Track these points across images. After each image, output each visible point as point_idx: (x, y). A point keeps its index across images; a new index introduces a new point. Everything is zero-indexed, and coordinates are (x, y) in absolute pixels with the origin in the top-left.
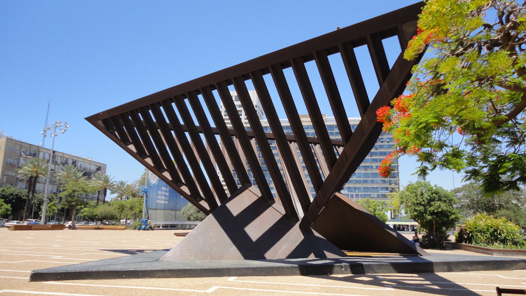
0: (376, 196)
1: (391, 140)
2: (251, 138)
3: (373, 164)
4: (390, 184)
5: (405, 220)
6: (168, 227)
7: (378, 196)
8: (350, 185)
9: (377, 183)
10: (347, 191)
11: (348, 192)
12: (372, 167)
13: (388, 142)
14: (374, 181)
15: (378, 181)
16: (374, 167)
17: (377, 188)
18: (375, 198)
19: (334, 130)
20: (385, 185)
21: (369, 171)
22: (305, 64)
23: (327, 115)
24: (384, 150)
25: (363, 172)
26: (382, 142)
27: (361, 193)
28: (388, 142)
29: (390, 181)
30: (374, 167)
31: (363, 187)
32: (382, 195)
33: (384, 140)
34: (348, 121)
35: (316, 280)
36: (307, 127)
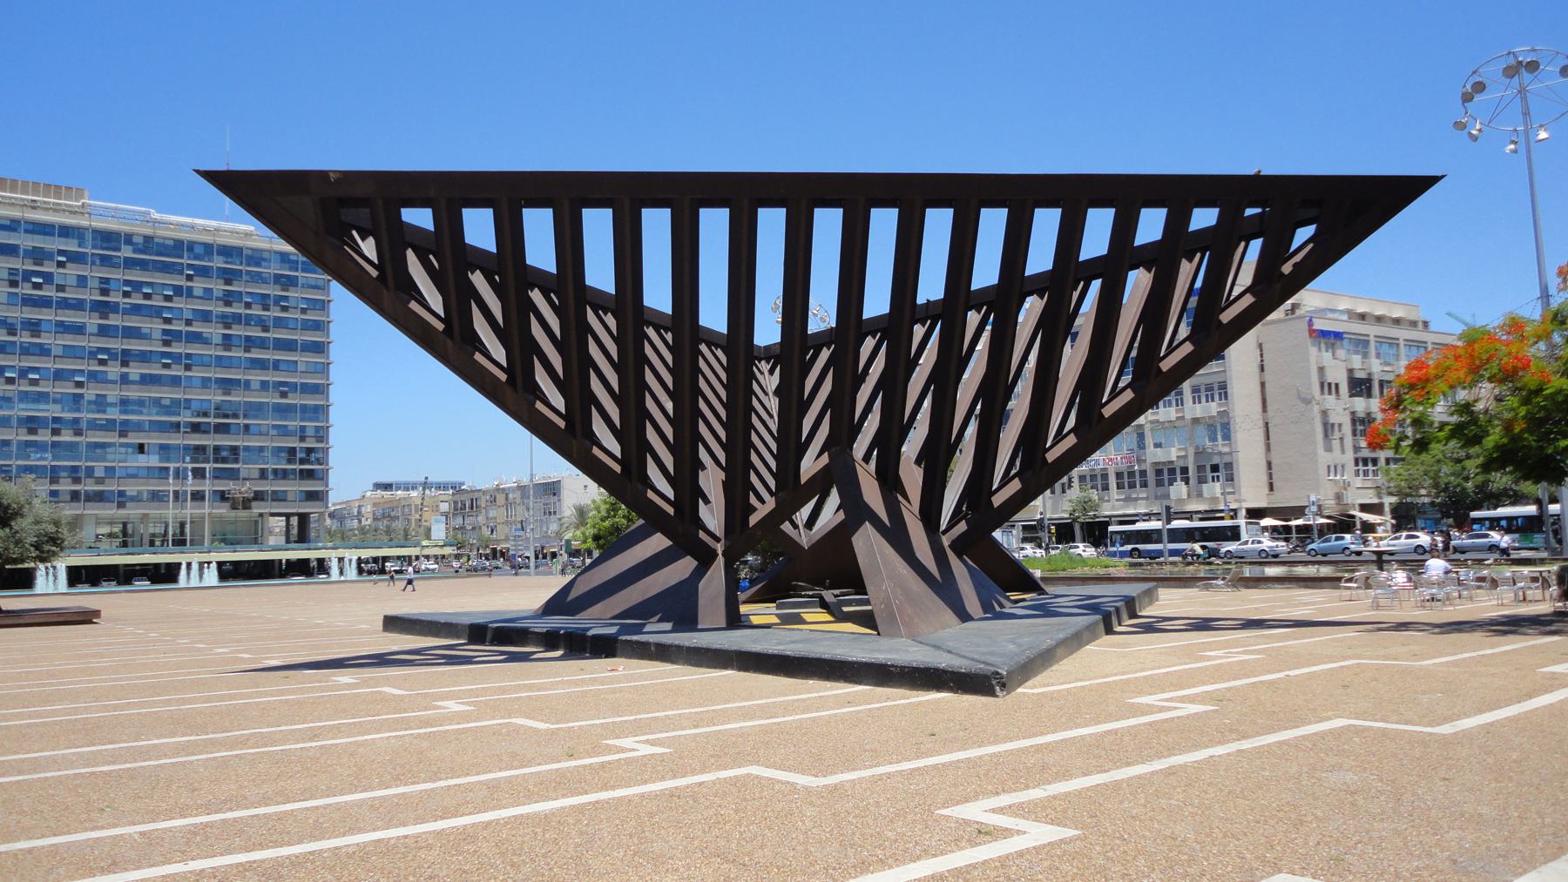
0: (256, 474)
1: (311, 307)
2: (768, 353)
3: (251, 375)
4: (302, 439)
5: (377, 544)
6: (1271, 473)
7: (263, 474)
8: (170, 439)
9: (260, 434)
10: (157, 457)
11: (161, 461)
12: (247, 384)
13: (304, 311)
14: (252, 429)
15: (264, 429)
16: (255, 386)
17: (261, 449)
18: (252, 481)
19: (119, 249)
20: (288, 442)
21: (236, 397)
22: (760, 210)
23: (86, 194)
24: (288, 334)
25: (215, 398)
26: (285, 309)
27: (178, 465)
28: (304, 311)
29: (303, 429)
30: (255, 386)
31: (19, 441)
32: (275, 471)
33: (292, 303)
34: (783, 323)
35: (872, 589)
36: (8, 223)
